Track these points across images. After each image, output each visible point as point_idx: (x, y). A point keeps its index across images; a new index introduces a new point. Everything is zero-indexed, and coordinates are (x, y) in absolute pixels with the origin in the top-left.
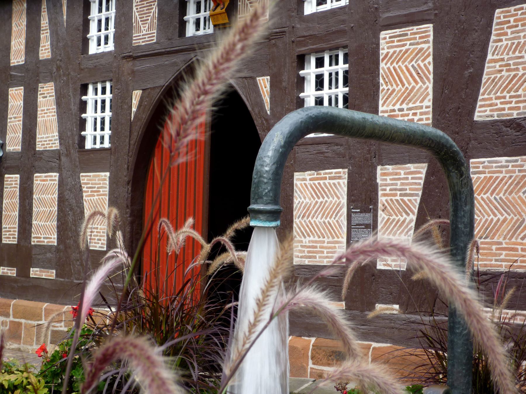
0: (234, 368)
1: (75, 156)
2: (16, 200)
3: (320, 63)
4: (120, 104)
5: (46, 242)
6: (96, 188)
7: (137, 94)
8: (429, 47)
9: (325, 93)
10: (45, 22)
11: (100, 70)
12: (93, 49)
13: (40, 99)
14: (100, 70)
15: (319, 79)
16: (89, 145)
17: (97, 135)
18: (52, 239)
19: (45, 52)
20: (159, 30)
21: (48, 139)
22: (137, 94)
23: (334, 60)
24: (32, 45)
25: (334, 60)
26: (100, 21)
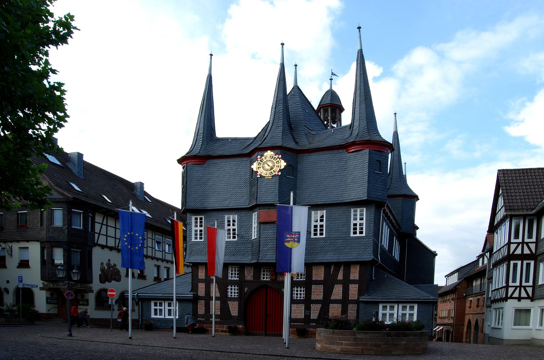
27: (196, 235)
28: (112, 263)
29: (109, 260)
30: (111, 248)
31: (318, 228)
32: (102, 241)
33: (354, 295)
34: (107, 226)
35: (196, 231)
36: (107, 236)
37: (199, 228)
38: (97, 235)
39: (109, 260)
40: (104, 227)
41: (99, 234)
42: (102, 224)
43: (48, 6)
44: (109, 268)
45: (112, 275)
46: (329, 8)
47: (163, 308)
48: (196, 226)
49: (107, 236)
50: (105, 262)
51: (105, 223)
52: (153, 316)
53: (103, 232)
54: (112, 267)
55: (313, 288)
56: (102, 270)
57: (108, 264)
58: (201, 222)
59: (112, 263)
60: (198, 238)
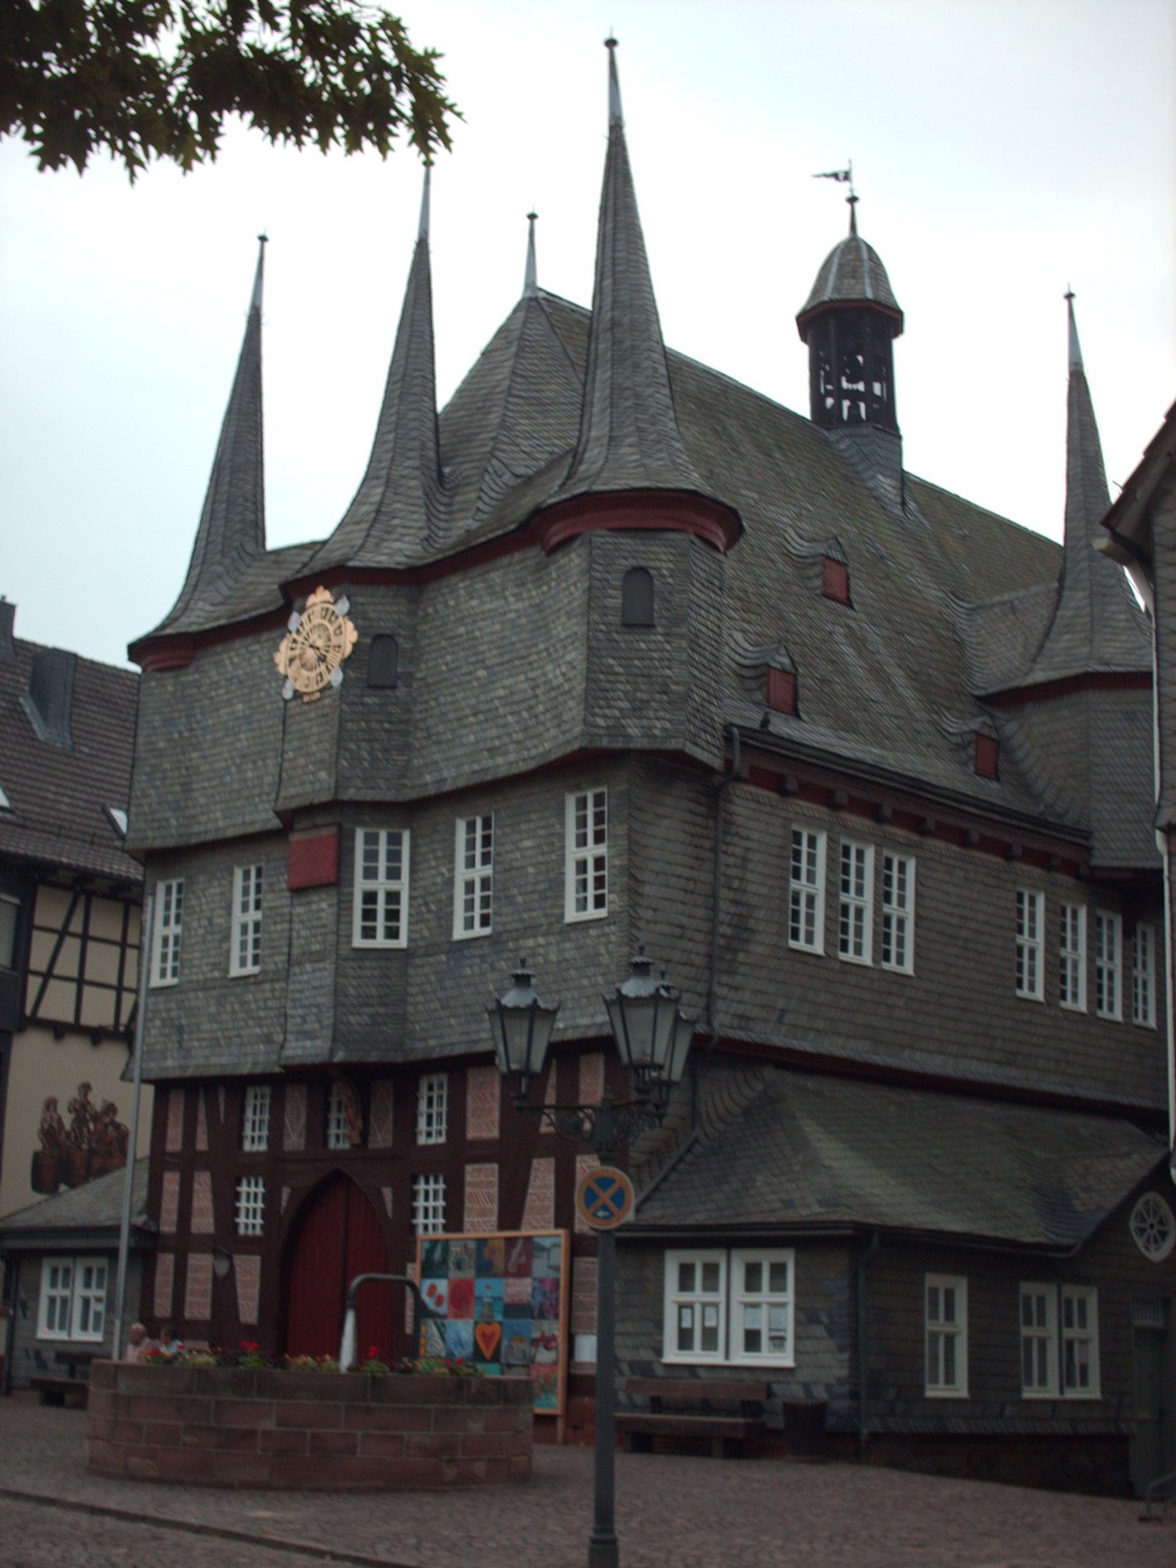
0: (209, 837)
1: (226, 1241)
2: (171, 1278)
3: (427, 1182)
4: (270, 1199)
5: (199, 1316)
6: (249, 1272)
7: (286, 1192)
8: (495, 1179)
9: (431, 1221)
10: (202, 1117)
11: (252, 1167)
12: (248, 1146)
13: (196, 1186)
14: (252, 1167)
15: (427, 1193)
16: (242, 1231)
17: (250, 1222)
18: (205, 1313)
19: (202, 1144)
20: (307, 1140)
21: (203, 1222)
22: (286, 1192)
23: (436, 1182)
24: (189, 1136)
25: (436, 1182)
26: (254, 1122)
27: (369, 915)
28: (97, 1101)
29: (86, 1088)
30: (97, 1036)
31: (381, 907)
32: (57, 1004)
33: (478, 1185)
34: (85, 937)
35: (370, 898)
36: (80, 981)
37: (382, 885)
38: (34, 983)
39: (86, 1088)
40: (72, 946)
41: (47, 976)
42: (63, 933)
43: (137, 44)
44: (80, 1121)
45: (91, 1152)
46: (349, 152)
47: (720, 1297)
48: (370, 873)
49: (80, 981)
50: (66, 1095)
51: (76, 926)
52: (672, 1355)
53: (67, 964)
54: (96, 1118)
55: (468, 1178)
56: (50, 1133)
57: (81, 1108)
58: (394, 856)
59: (97, 1101)
60: (380, 932)
